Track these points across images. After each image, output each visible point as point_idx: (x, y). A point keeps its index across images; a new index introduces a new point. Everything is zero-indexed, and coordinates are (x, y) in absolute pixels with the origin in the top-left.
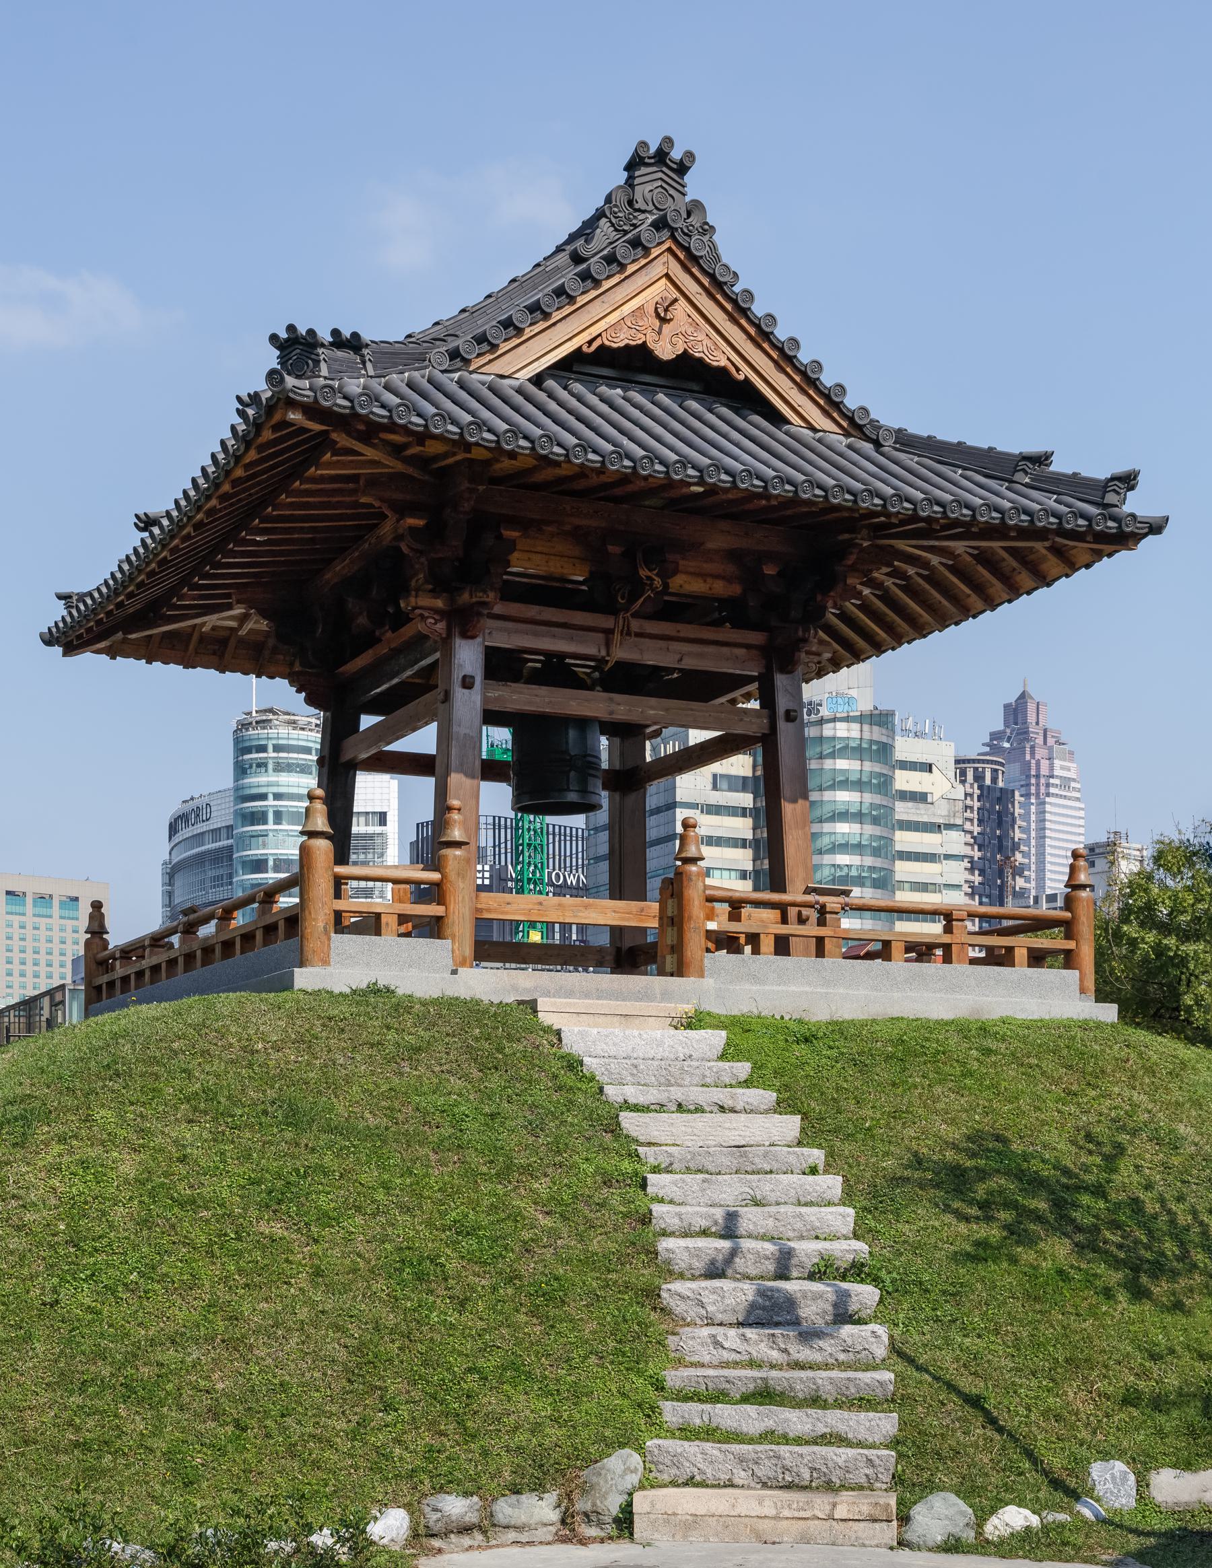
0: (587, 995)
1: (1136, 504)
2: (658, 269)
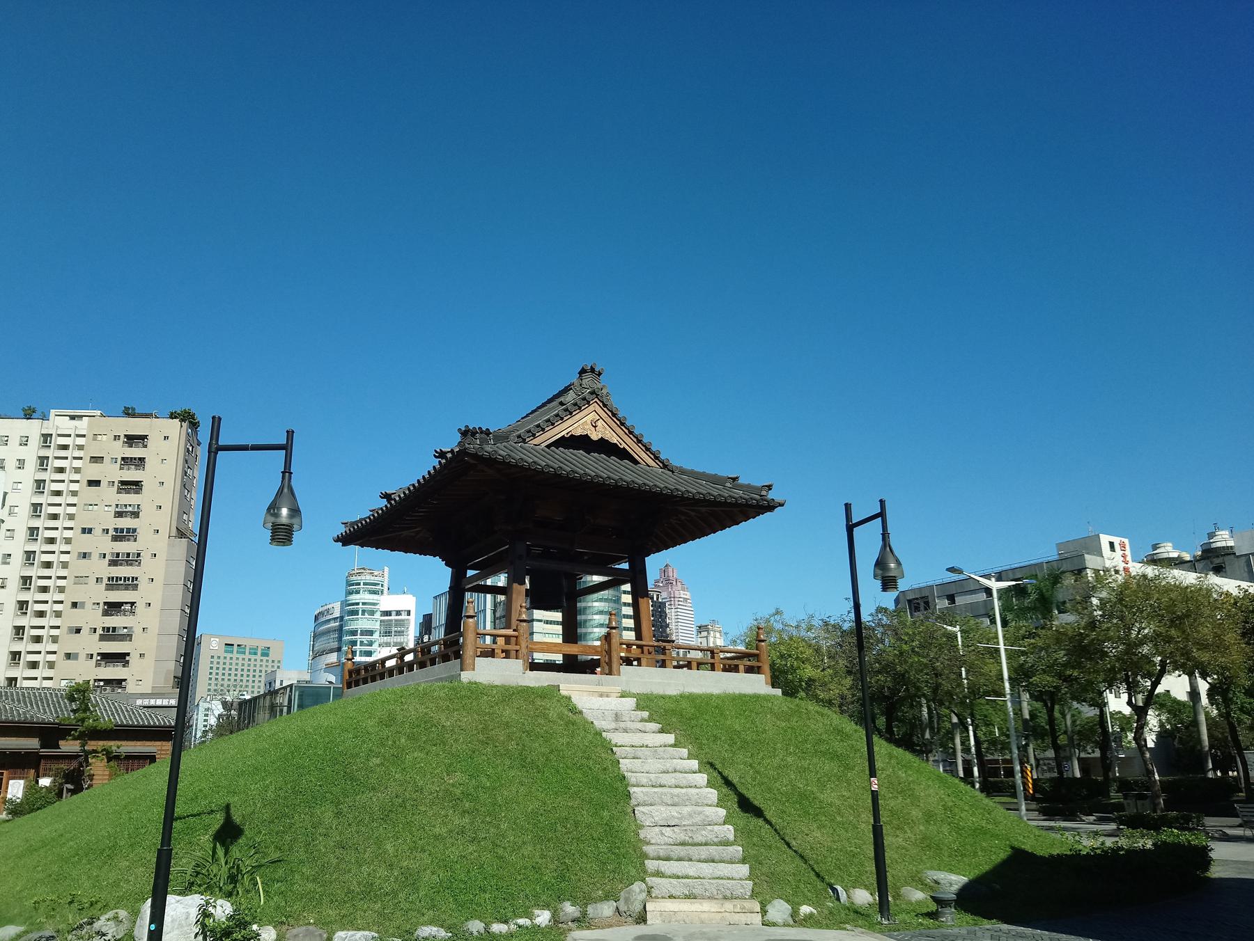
1: (771, 495)
2: (591, 408)
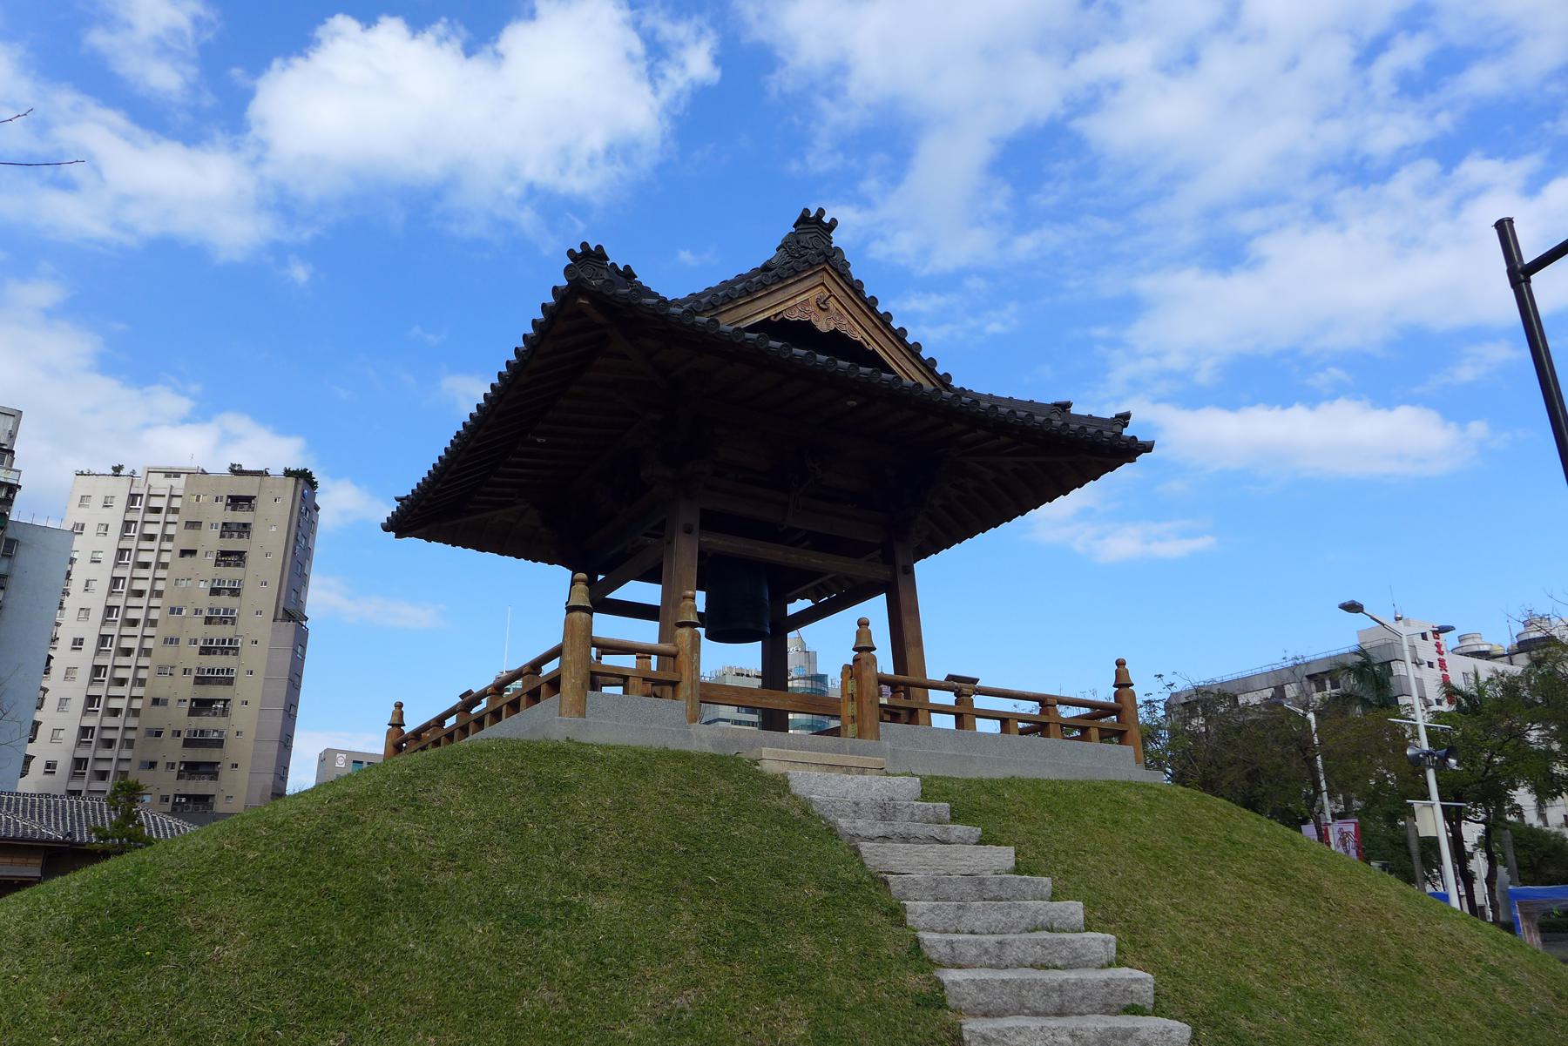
0: (833, 751)
